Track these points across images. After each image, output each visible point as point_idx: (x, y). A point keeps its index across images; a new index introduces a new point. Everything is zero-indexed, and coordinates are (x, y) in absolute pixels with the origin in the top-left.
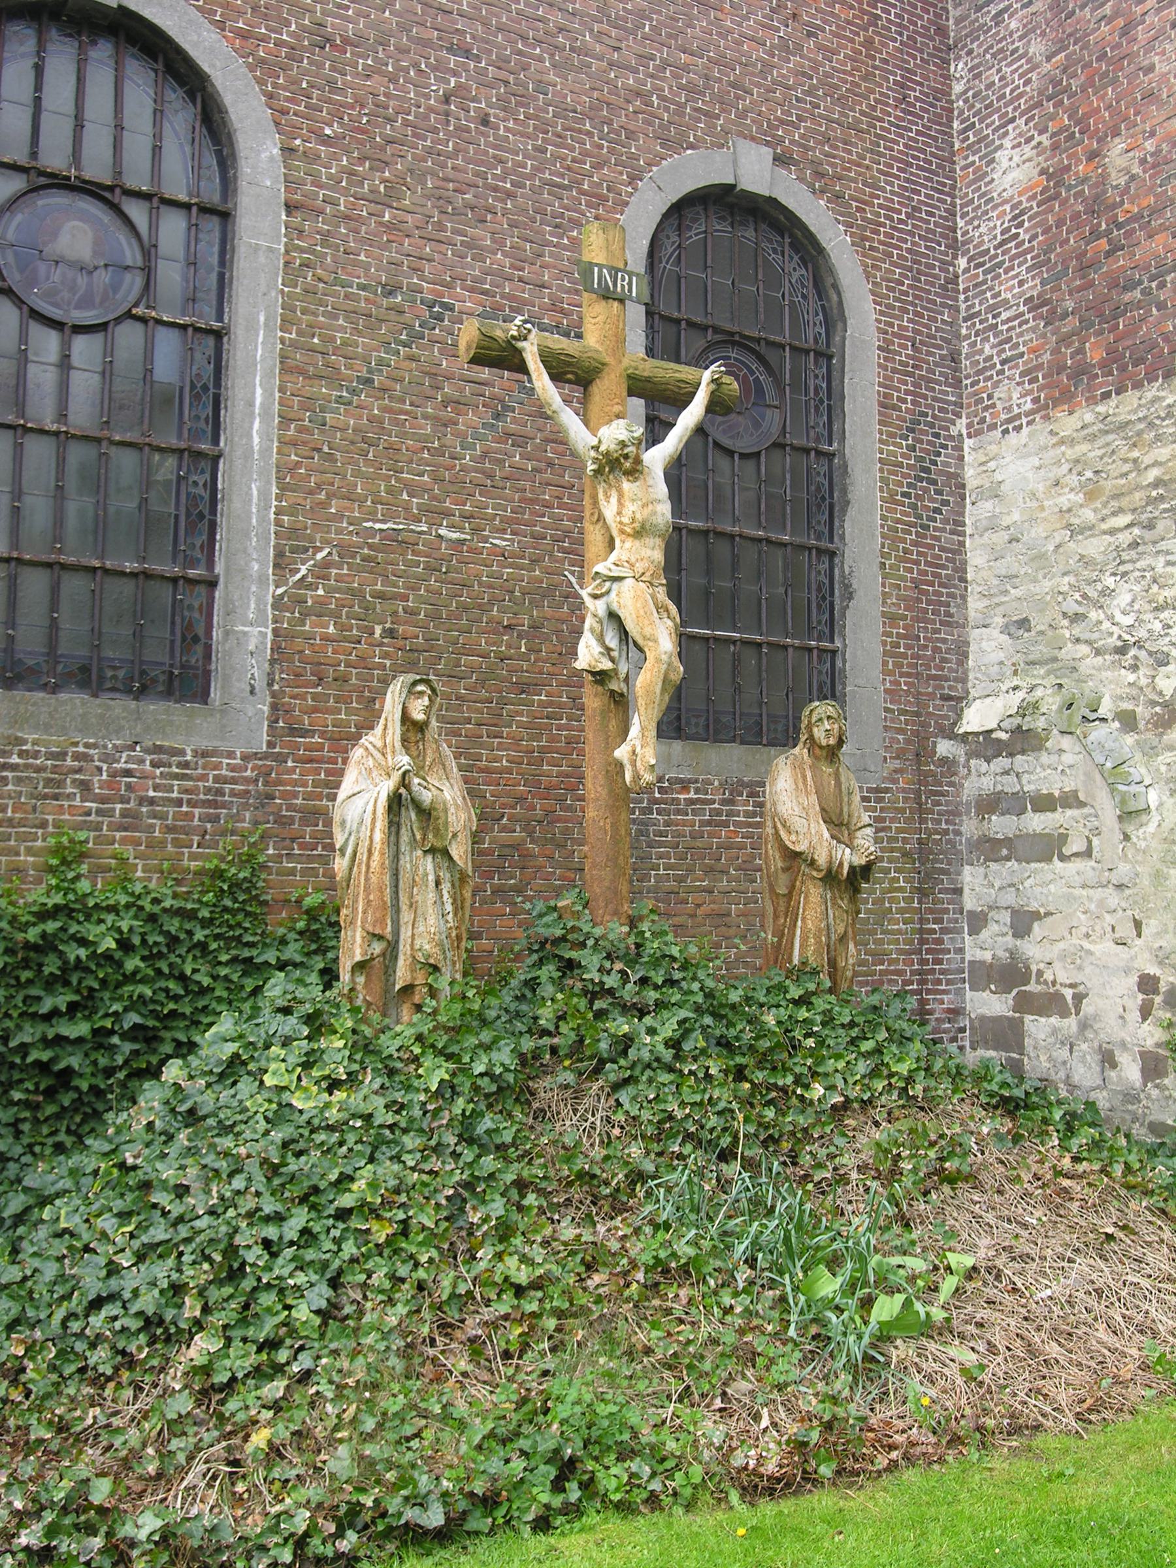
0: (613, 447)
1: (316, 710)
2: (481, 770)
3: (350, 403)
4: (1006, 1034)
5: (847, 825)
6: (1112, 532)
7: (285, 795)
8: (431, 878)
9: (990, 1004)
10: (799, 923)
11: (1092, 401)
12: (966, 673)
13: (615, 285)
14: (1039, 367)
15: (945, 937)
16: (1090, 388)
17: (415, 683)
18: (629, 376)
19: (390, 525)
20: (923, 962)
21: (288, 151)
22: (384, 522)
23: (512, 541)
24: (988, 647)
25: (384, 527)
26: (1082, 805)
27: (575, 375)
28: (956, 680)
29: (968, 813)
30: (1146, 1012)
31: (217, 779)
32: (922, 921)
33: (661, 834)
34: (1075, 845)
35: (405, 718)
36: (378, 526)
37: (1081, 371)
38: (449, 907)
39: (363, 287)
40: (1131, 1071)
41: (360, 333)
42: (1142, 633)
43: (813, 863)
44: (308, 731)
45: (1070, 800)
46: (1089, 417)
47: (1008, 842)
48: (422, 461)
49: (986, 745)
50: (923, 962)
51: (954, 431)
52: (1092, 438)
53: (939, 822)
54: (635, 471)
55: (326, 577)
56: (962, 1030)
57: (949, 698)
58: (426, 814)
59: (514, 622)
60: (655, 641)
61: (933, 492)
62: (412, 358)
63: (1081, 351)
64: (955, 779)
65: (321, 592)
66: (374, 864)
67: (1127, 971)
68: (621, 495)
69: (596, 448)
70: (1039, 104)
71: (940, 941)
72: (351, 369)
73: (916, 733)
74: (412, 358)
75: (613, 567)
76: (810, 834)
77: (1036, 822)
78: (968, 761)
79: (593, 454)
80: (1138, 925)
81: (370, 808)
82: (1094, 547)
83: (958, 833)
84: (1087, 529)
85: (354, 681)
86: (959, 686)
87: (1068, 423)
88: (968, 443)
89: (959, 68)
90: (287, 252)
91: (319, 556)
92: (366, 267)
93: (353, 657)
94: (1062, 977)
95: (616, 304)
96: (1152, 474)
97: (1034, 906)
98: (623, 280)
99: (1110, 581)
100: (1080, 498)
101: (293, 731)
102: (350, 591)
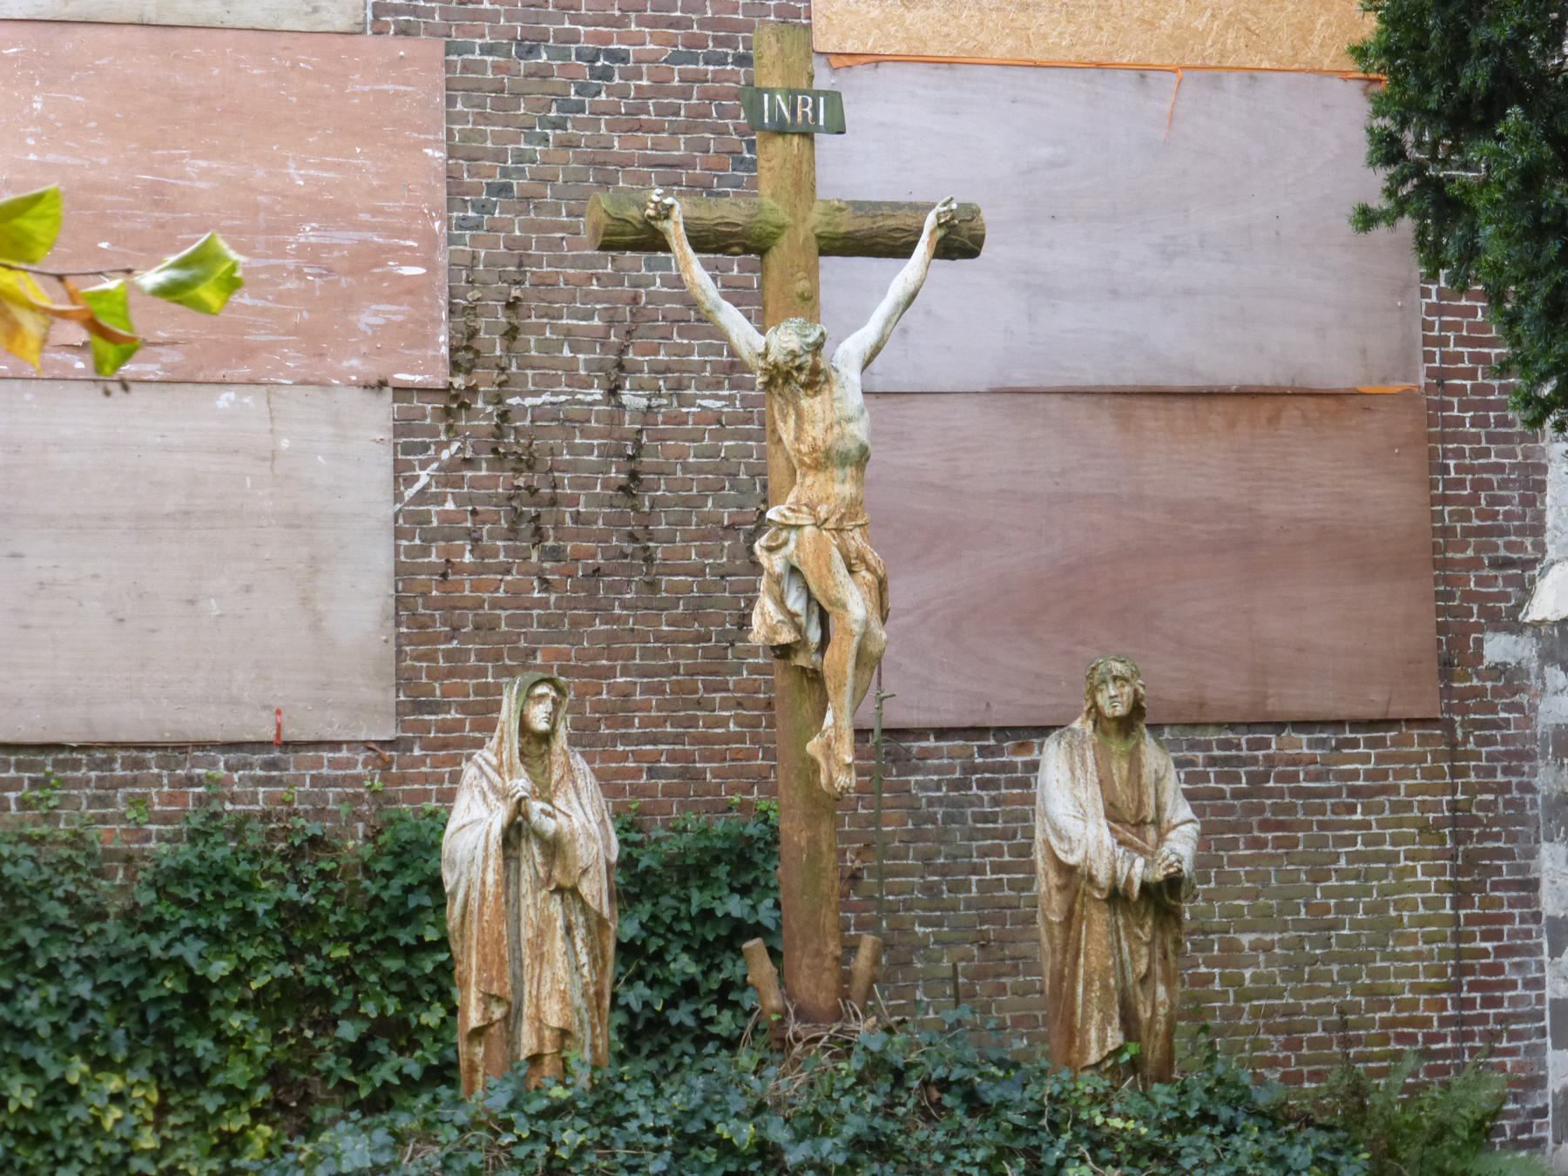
0: (781, 359)
1: (451, 673)
2: (696, 740)
3: (478, 227)
5: (1157, 822)
7: (412, 797)
8: (560, 923)
10: (1082, 960)
12: (1540, 516)
13: (794, 113)
15: (1506, 962)
17: (535, 684)
18: (819, 237)
19: (546, 398)
22: (537, 394)
23: (731, 399)
25: (538, 401)
28: (1520, 531)
29: (1544, 755)
31: (315, 780)
32: (1458, 937)
33: (985, 818)
35: (524, 728)
36: (529, 401)
38: (584, 959)
39: (488, 50)
41: (487, 119)
43: (1091, 879)
44: (438, 703)
53: (1491, 772)
55: (458, 483)
56: (1542, 1113)
57: (1508, 563)
58: (553, 848)
59: (738, 519)
60: (844, 606)
62: (566, 144)
64: (1523, 698)
65: (450, 506)
66: (487, 911)
68: (799, 416)
69: (764, 355)
71: (1497, 969)
72: (477, 175)
74: (566, 144)
75: (788, 513)
78: (1541, 668)
79: (761, 364)
81: (481, 844)
83: (1527, 788)
85: (504, 628)
86: (1528, 541)
90: (376, 17)
91: (445, 455)
92: (493, 16)
93: (501, 594)
95: (796, 139)
98: (805, 104)
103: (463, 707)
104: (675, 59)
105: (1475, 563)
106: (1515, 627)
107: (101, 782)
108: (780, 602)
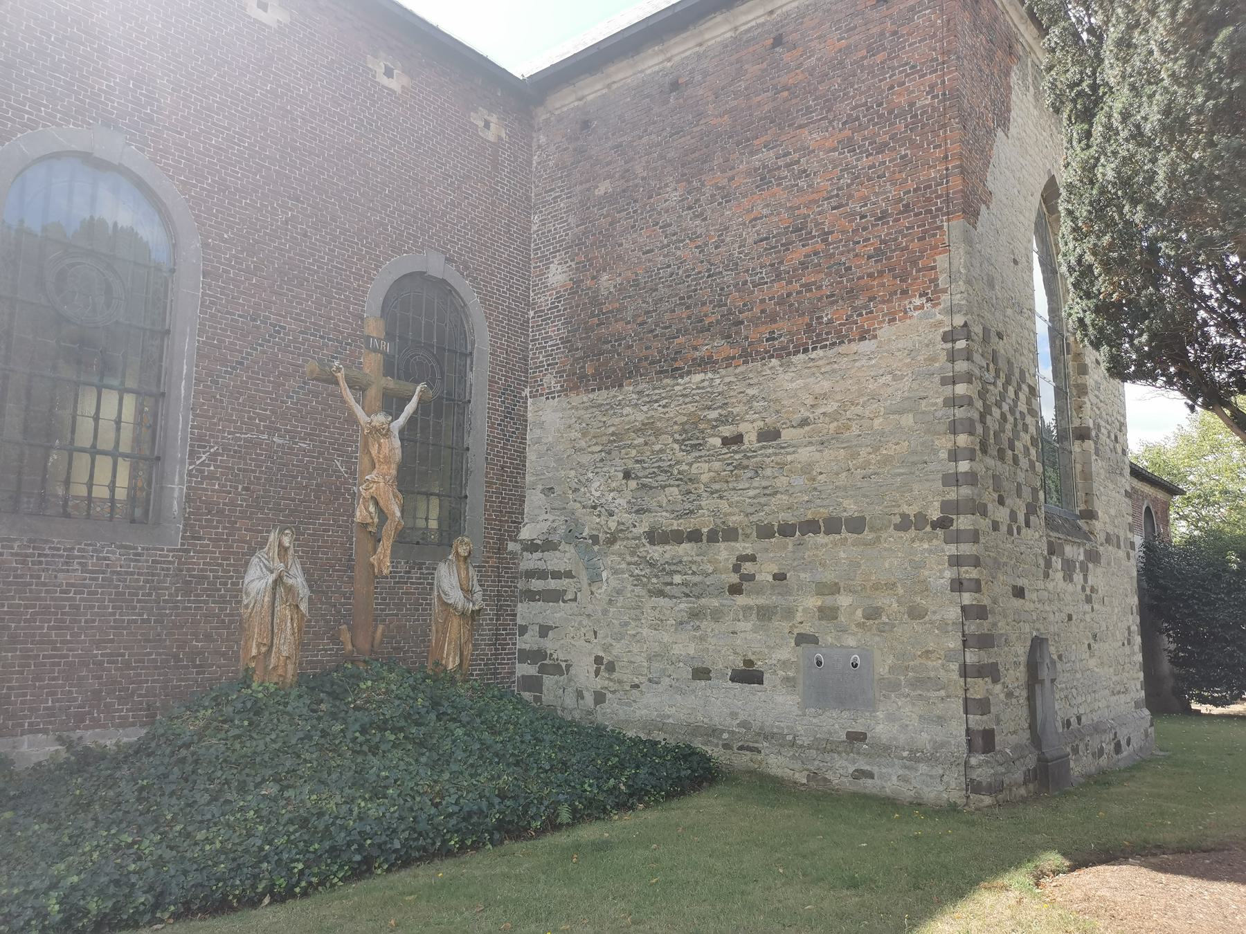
4: (533, 684)
6: (593, 453)
7: (188, 570)
9: (525, 669)
11: (587, 391)
14: (564, 371)
16: (586, 386)
20: (496, 649)
21: (205, 245)
24: (534, 499)
26: (573, 577)
27: (358, 387)
30: (597, 673)
34: (569, 596)
35: (280, 545)
37: (583, 377)
39: (240, 316)
40: (589, 699)
41: (238, 339)
42: (603, 501)
45: (569, 574)
46: (585, 399)
47: (539, 593)
48: (267, 404)
49: (531, 547)
50: (496, 649)
51: (523, 394)
52: (587, 409)
54: (387, 434)
58: (290, 589)
61: (513, 422)
62: (264, 352)
63: (583, 367)
67: (590, 654)
70: (571, 247)
73: (499, 539)
76: (456, 597)
77: (553, 584)
80: (595, 633)
82: (585, 459)
84: (581, 450)
87: (575, 399)
88: (530, 401)
89: (536, 218)
94: (561, 657)
96: (612, 429)
97: (550, 623)
99: (590, 475)
100: (579, 435)
101: (194, 538)
102: (227, 468)
103: (209, 539)
104: (301, 332)
105: (507, 521)
106: (516, 541)
107: (68, 557)
108: (367, 509)
